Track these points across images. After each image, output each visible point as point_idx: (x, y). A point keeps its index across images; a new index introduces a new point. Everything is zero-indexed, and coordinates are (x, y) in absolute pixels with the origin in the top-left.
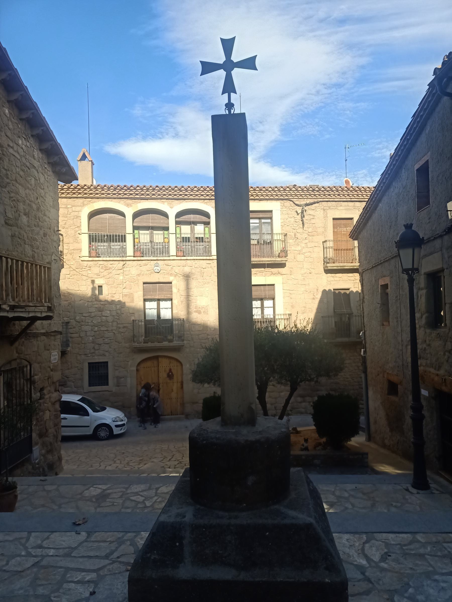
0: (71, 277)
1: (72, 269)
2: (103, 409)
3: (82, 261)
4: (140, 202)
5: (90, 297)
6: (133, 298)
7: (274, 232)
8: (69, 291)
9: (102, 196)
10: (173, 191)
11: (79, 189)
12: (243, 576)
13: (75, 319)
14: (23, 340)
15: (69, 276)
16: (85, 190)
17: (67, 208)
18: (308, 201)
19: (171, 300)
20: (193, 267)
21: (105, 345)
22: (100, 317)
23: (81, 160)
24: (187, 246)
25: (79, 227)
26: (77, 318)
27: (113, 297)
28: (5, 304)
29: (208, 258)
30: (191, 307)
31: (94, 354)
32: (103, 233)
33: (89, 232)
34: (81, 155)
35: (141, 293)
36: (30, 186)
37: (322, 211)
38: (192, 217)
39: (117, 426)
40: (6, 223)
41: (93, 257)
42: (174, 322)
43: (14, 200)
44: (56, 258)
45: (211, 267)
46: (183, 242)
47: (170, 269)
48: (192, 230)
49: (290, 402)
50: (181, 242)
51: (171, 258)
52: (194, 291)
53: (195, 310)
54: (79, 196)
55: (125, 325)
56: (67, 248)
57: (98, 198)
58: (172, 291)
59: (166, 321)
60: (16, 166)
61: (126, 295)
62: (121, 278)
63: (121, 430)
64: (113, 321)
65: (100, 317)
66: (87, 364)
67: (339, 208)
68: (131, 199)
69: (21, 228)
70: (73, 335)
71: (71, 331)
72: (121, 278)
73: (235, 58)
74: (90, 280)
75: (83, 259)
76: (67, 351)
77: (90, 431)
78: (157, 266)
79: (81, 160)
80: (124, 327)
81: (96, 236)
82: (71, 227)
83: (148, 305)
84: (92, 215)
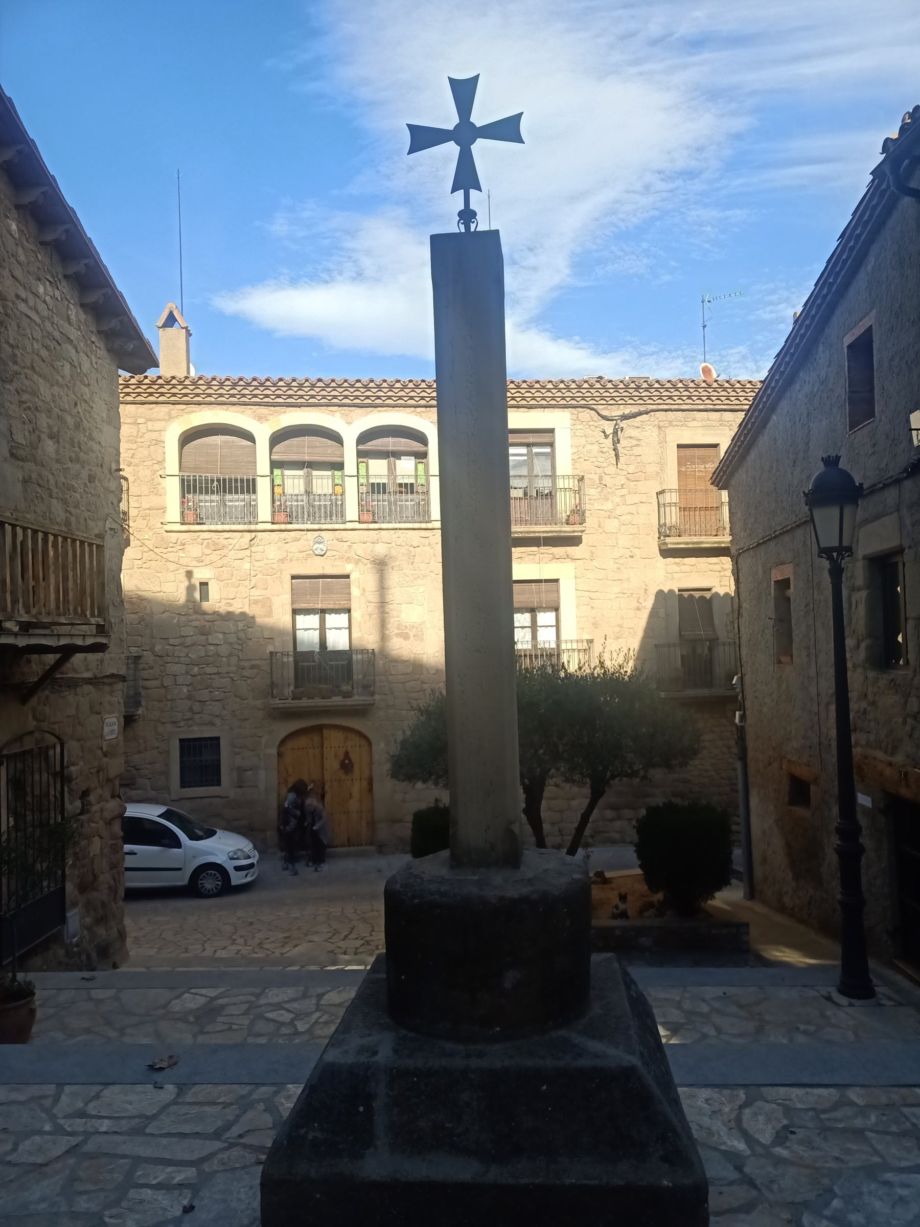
0: (144, 565)
1: (146, 549)
2: (210, 834)
3: (167, 532)
4: (285, 412)
5: (184, 606)
6: (270, 607)
7: (558, 473)
8: (140, 593)
9: (208, 399)
10: (352, 390)
11: (162, 386)
12: (495, 1174)
13: (152, 650)
14: (47, 692)
15: (140, 562)
16: (174, 386)
17: (135, 423)
18: (627, 410)
19: (349, 611)
20: (393, 544)
21: (214, 703)
22: (204, 646)
23: (165, 325)
24: (380, 502)
25: (161, 462)
26: (158, 648)
27: (231, 605)
28: (10, 619)
29: (423, 525)
30: (389, 626)
31: (190, 722)
32: (209, 475)
33: (181, 474)
34: (165, 315)
35: (287, 597)
36: (60, 379)
37: (656, 430)
38: (390, 443)
39: (238, 868)
40: (12, 455)
41: (189, 524)
42: (354, 657)
43: (29, 408)
44: (114, 526)
45: (429, 544)
46: (373, 492)
47: (346, 548)
48: (392, 469)
49: (591, 820)
50: (368, 492)
51: (349, 526)
52: (396, 594)
53: (396, 631)
54: (161, 399)
55: (254, 662)
56: (136, 505)
57: (199, 404)
58: (350, 594)
59: (338, 654)
60: (33, 339)
61: (256, 602)
62: (247, 566)
63: (246, 876)
64: (230, 655)
65: (204, 646)
66: (178, 743)
67: (691, 424)
68: (267, 405)
69: (43, 465)
70: (148, 683)
71: (144, 674)
72: (247, 566)
73: (479, 118)
74: (182, 571)
75: (168, 527)
76: (136, 715)
77: (182, 879)
78: (320, 543)
79: (165, 325)
80: (253, 667)
81: (195, 480)
82: (145, 464)
83: (302, 621)
84: (187, 438)
